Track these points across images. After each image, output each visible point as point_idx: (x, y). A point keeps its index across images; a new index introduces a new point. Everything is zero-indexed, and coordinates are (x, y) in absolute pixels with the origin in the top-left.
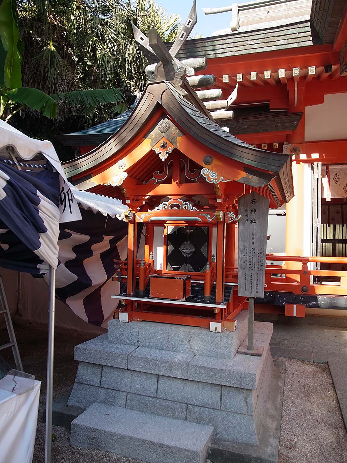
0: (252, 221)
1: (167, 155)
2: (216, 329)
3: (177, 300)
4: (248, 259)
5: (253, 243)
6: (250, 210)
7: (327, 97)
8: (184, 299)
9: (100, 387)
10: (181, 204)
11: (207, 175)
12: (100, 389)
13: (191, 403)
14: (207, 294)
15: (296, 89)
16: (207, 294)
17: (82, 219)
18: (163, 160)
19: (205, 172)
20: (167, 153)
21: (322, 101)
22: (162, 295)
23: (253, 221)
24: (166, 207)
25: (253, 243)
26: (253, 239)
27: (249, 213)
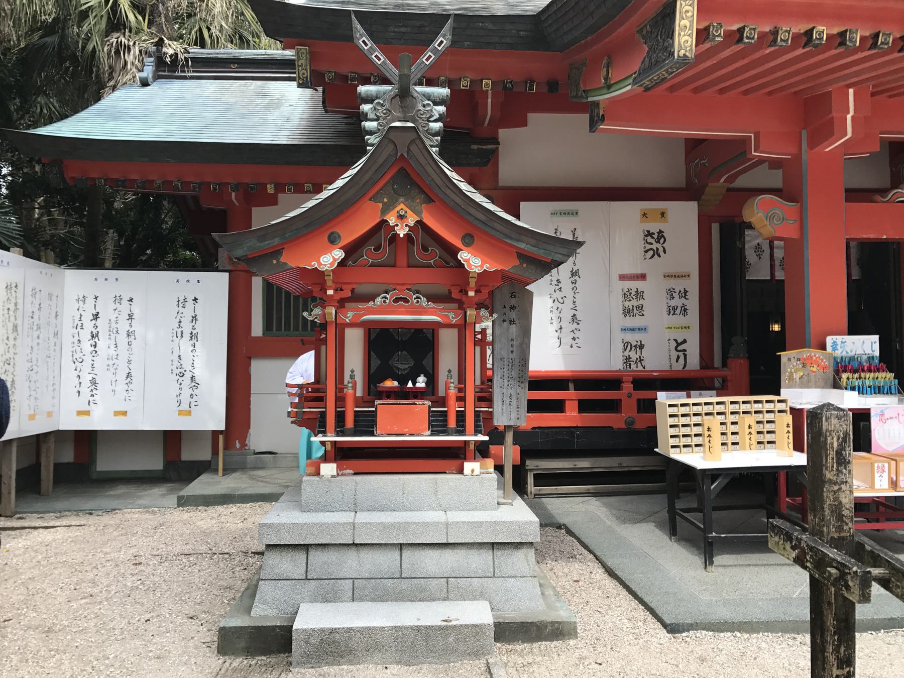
0: (510, 321)
2: (473, 471)
3: (419, 435)
4: (505, 374)
5: (512, 352)
6: (508, 307)
7: (532, 117)
8: (429, 432)
9: (307, 579)
10: (411, 298)
11: (468, 261)
12: (307, 582)
13: (453, 575)
14: (452, 423)
15: (489, 100)
16: (452, 423)
17: (876, 338)
18: (402, 236)
19: (464, 256)
20: (406, 225)
21: (524, 124)
22: (396, 430)
23: (512, 322)
24: (387, 301)
25: (512, 352)
26: (512, 346)
27: (507, 310)
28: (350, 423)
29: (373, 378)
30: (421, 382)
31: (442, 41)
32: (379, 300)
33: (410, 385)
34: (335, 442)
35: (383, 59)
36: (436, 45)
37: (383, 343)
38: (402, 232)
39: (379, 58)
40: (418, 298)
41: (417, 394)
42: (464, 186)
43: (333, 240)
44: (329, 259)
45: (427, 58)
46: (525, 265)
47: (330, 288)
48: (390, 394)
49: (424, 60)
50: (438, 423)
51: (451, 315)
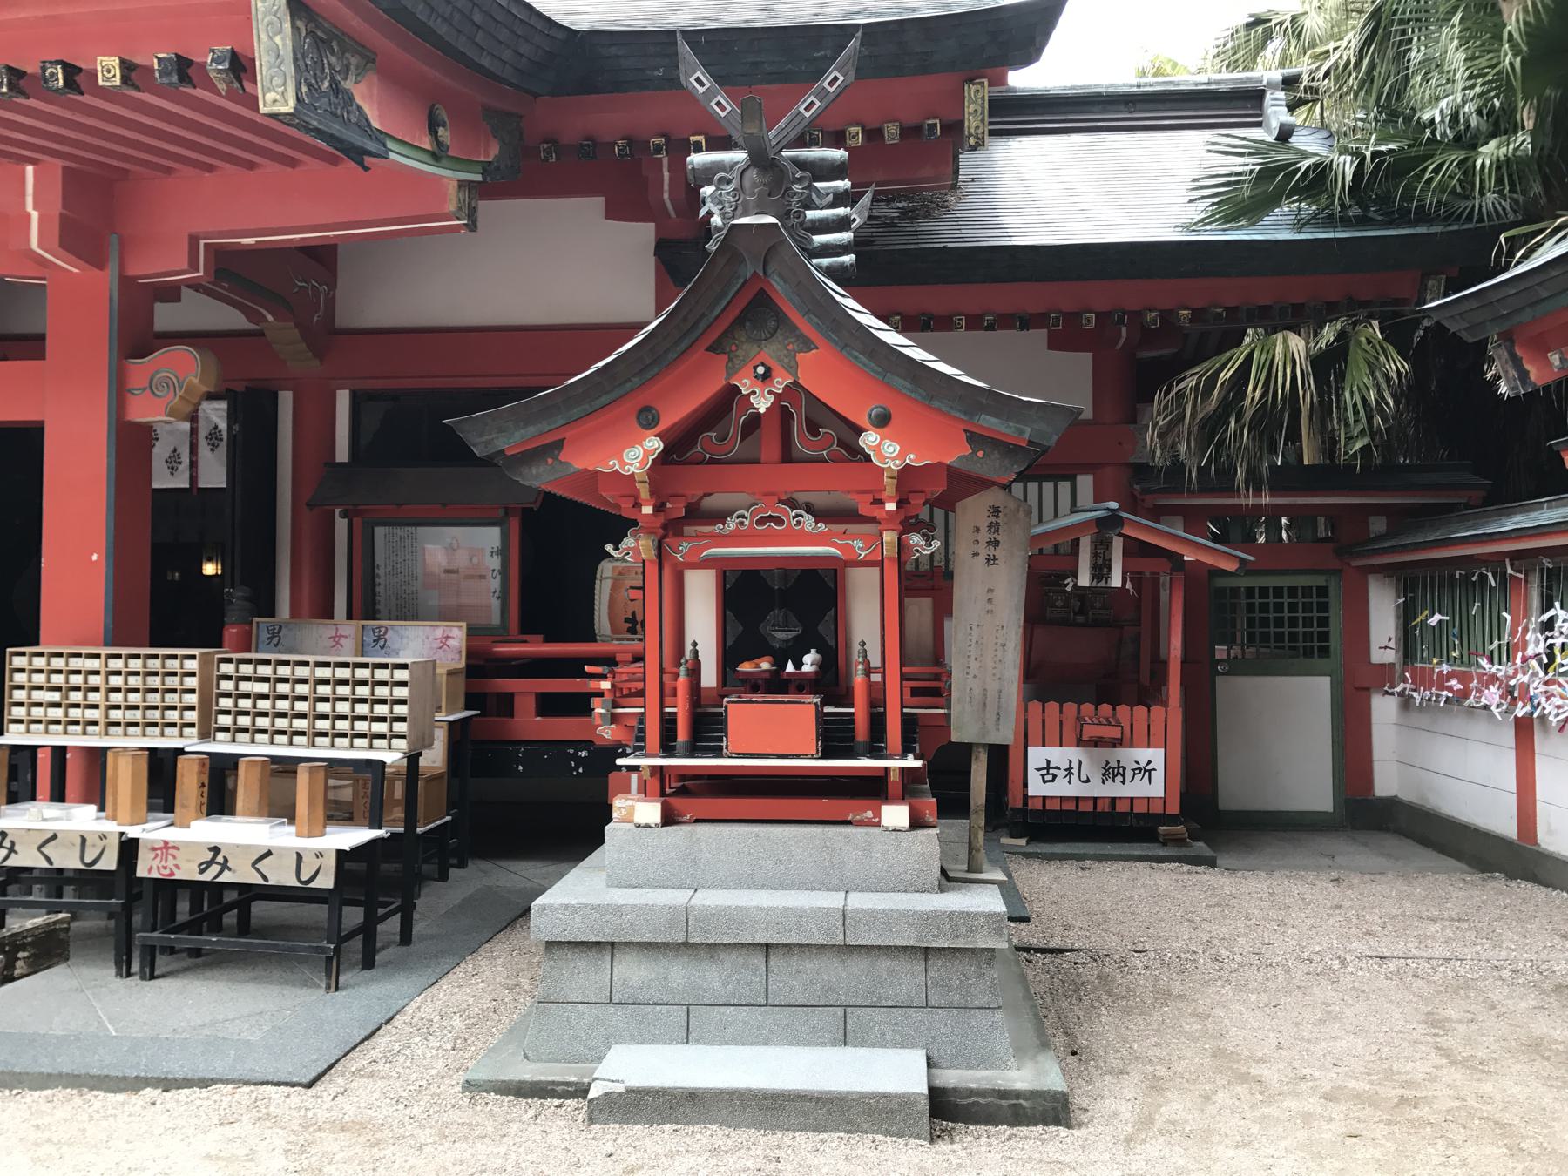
1: (772, 398)
11: (877, 449)
15: (666, 175)
20: (770, 392)
28: (682, 736)
29: (729, 657)
30: (810, 661)
31: (835, 79)
32: (731, 524)
33: (790, 668)
34: (661, 767)
35: (812, 98)
36: (719, 98)
37: (745, 594)
38: (762, 404)
39: (723, 106)
40: (798, 516)
41: (801, 685)
42: (867, 319)
43: (647, 418)
44: (638, 455)
45: (808, 106)
46: (980, 454)
47: (890, 499)
48: (755, 685)
49: (802, 109)
50: (834, 739)
51: (858, 544)
